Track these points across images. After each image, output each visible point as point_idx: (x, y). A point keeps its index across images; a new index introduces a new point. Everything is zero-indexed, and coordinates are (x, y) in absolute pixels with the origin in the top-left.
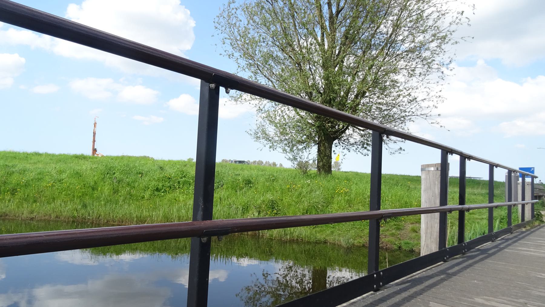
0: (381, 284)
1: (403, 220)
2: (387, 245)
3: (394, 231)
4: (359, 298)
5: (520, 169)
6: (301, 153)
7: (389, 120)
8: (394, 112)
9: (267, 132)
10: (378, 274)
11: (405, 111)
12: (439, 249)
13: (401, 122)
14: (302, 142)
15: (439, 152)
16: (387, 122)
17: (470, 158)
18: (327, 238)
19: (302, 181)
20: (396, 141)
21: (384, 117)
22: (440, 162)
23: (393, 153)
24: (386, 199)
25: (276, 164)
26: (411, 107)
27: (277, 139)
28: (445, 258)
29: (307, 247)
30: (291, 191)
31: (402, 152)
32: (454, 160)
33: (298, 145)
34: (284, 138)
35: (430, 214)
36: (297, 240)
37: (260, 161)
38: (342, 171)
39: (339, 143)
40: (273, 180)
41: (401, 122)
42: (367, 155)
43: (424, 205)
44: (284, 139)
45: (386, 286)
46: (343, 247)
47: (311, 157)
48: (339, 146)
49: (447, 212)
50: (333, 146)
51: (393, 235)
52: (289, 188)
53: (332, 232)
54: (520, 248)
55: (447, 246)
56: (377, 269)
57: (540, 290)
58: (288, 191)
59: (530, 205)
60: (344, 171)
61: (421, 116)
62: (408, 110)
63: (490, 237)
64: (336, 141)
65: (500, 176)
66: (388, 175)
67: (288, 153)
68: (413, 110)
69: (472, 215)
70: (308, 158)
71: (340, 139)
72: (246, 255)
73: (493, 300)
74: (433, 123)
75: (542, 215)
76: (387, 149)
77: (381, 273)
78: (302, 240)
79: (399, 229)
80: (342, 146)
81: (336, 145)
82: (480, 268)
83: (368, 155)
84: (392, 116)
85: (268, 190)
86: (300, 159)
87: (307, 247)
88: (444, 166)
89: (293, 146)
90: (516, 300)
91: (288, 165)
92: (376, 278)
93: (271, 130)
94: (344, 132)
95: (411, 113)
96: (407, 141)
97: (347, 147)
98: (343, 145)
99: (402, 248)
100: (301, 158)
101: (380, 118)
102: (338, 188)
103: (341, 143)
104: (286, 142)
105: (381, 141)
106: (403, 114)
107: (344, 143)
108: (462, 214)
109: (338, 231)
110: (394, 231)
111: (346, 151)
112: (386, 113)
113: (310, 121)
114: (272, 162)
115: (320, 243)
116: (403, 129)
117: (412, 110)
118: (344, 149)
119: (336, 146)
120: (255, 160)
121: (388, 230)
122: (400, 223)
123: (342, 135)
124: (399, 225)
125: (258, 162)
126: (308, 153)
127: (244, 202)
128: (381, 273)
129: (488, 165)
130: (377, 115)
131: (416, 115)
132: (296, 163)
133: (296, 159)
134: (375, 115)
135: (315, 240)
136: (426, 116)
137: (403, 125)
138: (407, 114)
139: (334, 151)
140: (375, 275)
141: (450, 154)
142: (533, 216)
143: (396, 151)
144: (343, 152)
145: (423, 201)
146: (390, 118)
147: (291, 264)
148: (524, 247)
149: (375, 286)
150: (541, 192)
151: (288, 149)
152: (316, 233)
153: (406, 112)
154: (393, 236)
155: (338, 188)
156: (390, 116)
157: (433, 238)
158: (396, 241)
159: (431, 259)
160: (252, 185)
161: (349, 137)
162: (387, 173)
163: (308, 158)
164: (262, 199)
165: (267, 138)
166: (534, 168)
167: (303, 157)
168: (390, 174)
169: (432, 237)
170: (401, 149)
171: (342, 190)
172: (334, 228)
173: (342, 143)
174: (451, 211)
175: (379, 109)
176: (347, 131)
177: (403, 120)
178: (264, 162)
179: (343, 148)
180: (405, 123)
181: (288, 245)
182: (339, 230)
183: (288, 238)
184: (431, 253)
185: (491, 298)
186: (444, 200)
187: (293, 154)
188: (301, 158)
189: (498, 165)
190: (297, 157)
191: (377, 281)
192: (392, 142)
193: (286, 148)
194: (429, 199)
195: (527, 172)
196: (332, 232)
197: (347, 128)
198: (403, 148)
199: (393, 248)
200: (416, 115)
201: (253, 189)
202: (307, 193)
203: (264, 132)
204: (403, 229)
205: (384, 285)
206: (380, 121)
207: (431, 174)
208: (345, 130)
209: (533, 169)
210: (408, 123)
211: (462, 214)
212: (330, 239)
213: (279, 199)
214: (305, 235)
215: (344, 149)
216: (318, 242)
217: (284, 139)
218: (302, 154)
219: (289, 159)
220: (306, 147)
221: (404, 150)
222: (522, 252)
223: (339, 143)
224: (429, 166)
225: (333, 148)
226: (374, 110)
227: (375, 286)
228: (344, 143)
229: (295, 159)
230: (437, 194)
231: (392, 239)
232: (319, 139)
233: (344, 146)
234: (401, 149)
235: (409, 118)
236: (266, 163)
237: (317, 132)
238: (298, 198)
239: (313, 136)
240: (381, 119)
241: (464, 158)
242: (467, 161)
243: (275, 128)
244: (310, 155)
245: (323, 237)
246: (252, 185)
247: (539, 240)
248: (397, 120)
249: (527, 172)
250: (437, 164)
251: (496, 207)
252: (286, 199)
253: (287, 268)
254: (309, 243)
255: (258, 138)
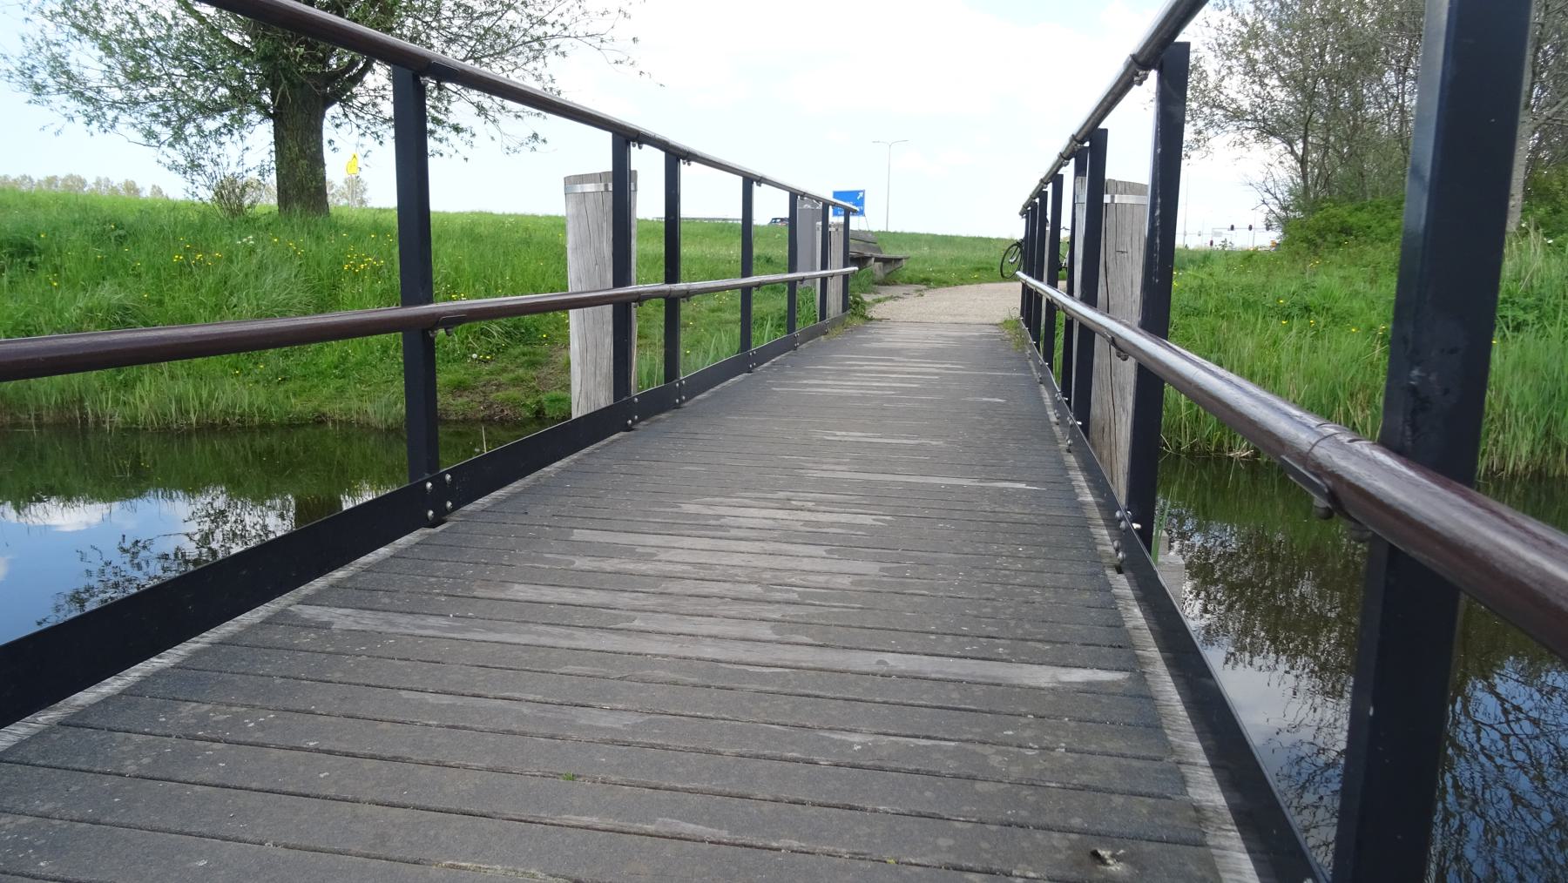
0: (449, 504)
1: (546, 339)
2: (502, 411)
3: (521, 371)
4: (383, 551)
5: (836, 194)
6: (214, 148)
7: (498, 49)
8: (510, 23)
9: (74, 70)
10: (438, 480)
11: (543, 22)
12: (615, 399)
13: (531, 54)
14: (220, 108)
15: (606, 137)
16: (492, 52)
17: (690, 157)
18: (326, 409)
19: (226, 240)
20: (522, 114)
21: (481, 39)
22: (610, 169)
23: (515, 151)
24: (496, 282)
25: (139, 186)
26: (558, 10)
27: (117, 95)
28: (630, 422)
29: (261, 443)
30: (191, 272)
31: (539, 146)
32: (647, 164)
33: (200, 120)
34: (144, 92)
35: (590, 309)
36: (225, 422)
37: (71, 177)
38: (372, 208)
39: (346, 115)
40: (121, 240)
41: (531, 54)
42: (438, 155)
43: (576, 285)
44: (146, 98)
45: (464, 508)
46: (376, 429)
47: (252, 160)
48: (348, 127)
49: (633, 304)
50: (327, 123)
51: (517, 382)
52: (182, 265)
53: (341, 391)
54: (805, 382)
55: (634, 392)
56: (434, 465)
57: (825, 467)
58: (180, 275)
59: (841, 279)
60: (376, 206)
61: (588, 40)
62: (549, 19)
63: (746, 360)
64: (334, 110)
65: (770, 207)
66: (510, 216)
67: (164, 147)
68: (566, 20)
69: (716, 314)
70: (240, 162)
71: (345, 104)
72: (51, 492)
73: (720, 504)
74: (621, 62)
75: (865, 303)
76: (493, 138)
77: (448, 477)
78: (243, 422)
79: (533, 364)
80: (358, 126)
81: (338, 122)
82: (708, 437)
83: (441, 155)
84: (506, 36)
85: (103, 272)
86: (216, 168)
87: (261, 443)
88: (621, 179)
89: (184, 120)
90: (769, 496)
91: (176, 188)
92: (432, 491)
93: (87, 60)
94: (358, 79)
95: (558, 28)
96: (550, 116)
97: (373, 129)
98: (360, 122)
99: (544, 414)
100: (217, 164)
101: (470, 38)
102: (351, 259)
103: (352, 116)
104: (154, 108)
105: (421, 93)
106: (538, 31)
107: (361, 114)
108: (672, 304)
109: (358, 385)
110: (521, 371)
111: (369, 140)
112: (486, 22)
113: (235, 38)
114: (122, 181)
115: (303, 425)
116: (539, 78)
117: (561, 20)
118: (364, 135)
119: (337, 126)
120: (50, 174)
121: (504, 370)
122: (539, 349)
123: (354, 90)
124: (534, 354)
125: (64, 180)
126: (241, 146)
127: (10, 317)
128: (448, 477)
129: (787, 194)
130: (460, 28)
131: (573, 35)
132: (200, 179)
133: (199, 165)
134: (455, 30)
135: (285, 418)
136: (602, 41)
137: (540, 64)
138: (548, 29)
139: (330, 142)
140: (429, 485)
141: (634, 146)
142: (846, 306)
143: (522, 144)
144: (362, 145)
145: (573, 277)
146: (497, 42)
147: (220, 503)
148: (815, 378)
149: (431, 513)
150: (870, 249)
151: (166, 134)
152: (288, 397)
153: (545, 23)
154: (518, 386)
155: (351, 259)
156: (499, 35)
157: (601, 375)
158: (527, 397)
159: (599, 426)
160: (37, 259)
161: (376, 97)
162: (507, 212)
163: (240, 162)
164: (81, 305)
165: (73, 86)
166: (863, 191)
167: (223, 160)
168: (516, 215)
169: (598, 372)
170: (535, 136)
171: (363, 262)
172: (344, 377)
173: (357, 116)
174: (640, 298)
175: (465, 11)
176: (368, 77)
177: (538, 46)
178: (91, 181)
179: (362, 132)
180: (544, 57)
181: (194, 439)
182: (361, 382)
183: (194, 419)
184: (597, 409)
185: (717, 499)
186: (622, 274)
187: (186, 149)
188: (217, 164)
189: (761, 178)
190: (201, 162)
191: (436, 501)
192: (512, 114)
193: (157, 128)
194: (589, 271)
195: (851, 202)
196: (341, 391)
197: (368, 67)
198: (541, 137)
199: (520, 415)
200: (573, 35)
201: (42, 274)
202: (246, 275)
203: (59, 67)
204: (547, 364)
205: (456, 507)
206: (469, 49)
207: (590, 204)
208: (363, 72)
209: (861, 194)
210: (551, 57)
211: (672, 304)
212: (334, 409)
213: (150, 301)
214: (251, 405)
215: (364, 135)
216: (292, 425)
217: (146, 98)
218: (221, 151)
219: (174, 167)
220: (232, 126)
221: (544, 141)
222: (808, 389)
223: (346, 115)
224: (583, 179)
225: (328, 131)
226: (449, 14)
227: (431, 513)
228: (361, 114)
229: (195, 166)
230: (607, 258)
231: (514, 393)
232: (273, 99)
233: (363, 127)
234: (535, 136)
235: (554, 42)
236: (98, 183)
237: (267, 77)
238: (217, 292)
239: (254, 91)
240: (472, 43)
241: (675, 157)
242: (635, 151)
243: (102, 53)
244: (247, 154)
245: (310, 406)
246: (37, 259)
247: (849, 359)
248: (521, 48)
249: (845, 201)
250: (604, 173)
251: (759, 285)
252: (174, 298)
253: (208, 515)
254: (265, 428)
255: (39, 89)
